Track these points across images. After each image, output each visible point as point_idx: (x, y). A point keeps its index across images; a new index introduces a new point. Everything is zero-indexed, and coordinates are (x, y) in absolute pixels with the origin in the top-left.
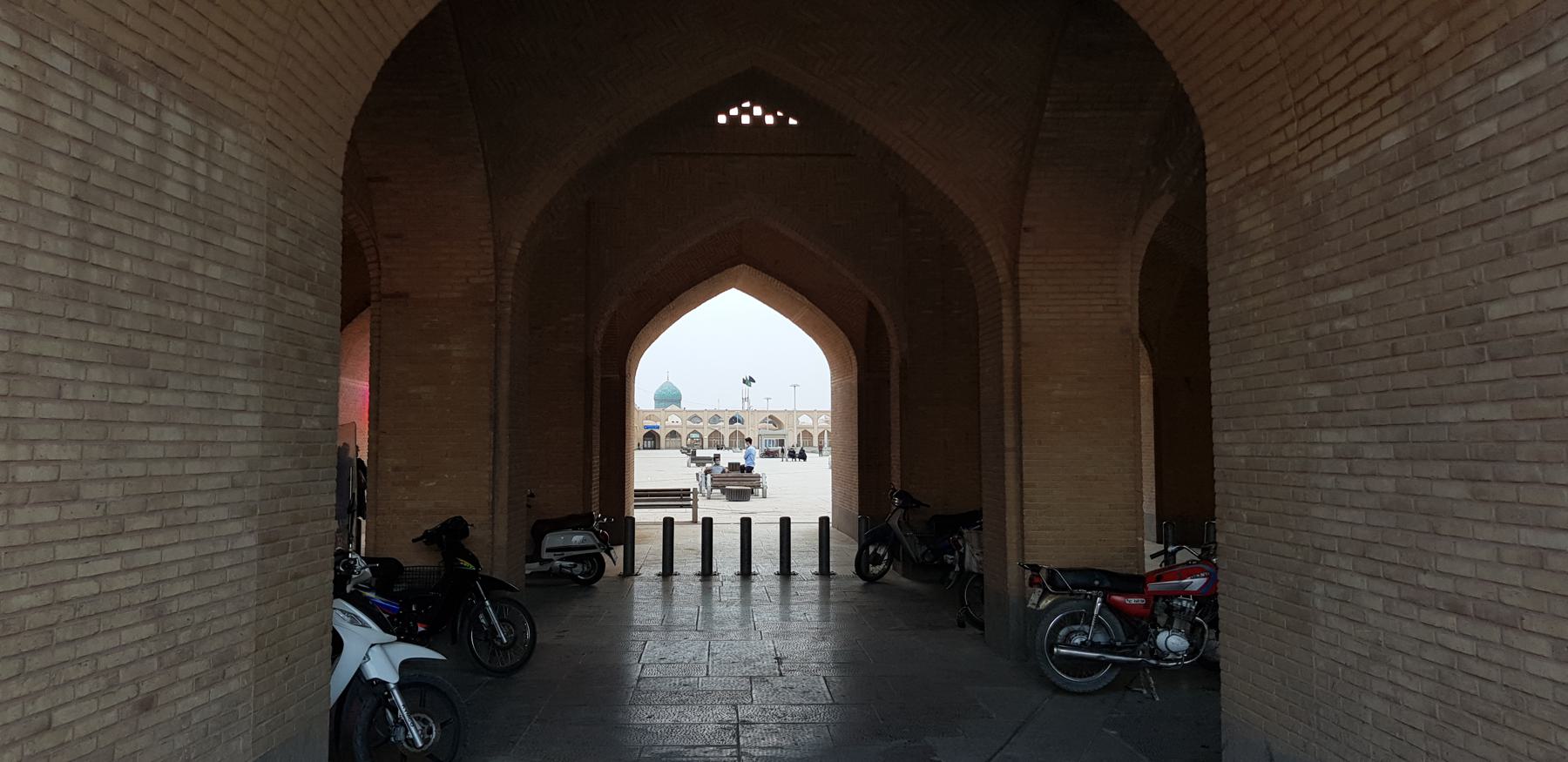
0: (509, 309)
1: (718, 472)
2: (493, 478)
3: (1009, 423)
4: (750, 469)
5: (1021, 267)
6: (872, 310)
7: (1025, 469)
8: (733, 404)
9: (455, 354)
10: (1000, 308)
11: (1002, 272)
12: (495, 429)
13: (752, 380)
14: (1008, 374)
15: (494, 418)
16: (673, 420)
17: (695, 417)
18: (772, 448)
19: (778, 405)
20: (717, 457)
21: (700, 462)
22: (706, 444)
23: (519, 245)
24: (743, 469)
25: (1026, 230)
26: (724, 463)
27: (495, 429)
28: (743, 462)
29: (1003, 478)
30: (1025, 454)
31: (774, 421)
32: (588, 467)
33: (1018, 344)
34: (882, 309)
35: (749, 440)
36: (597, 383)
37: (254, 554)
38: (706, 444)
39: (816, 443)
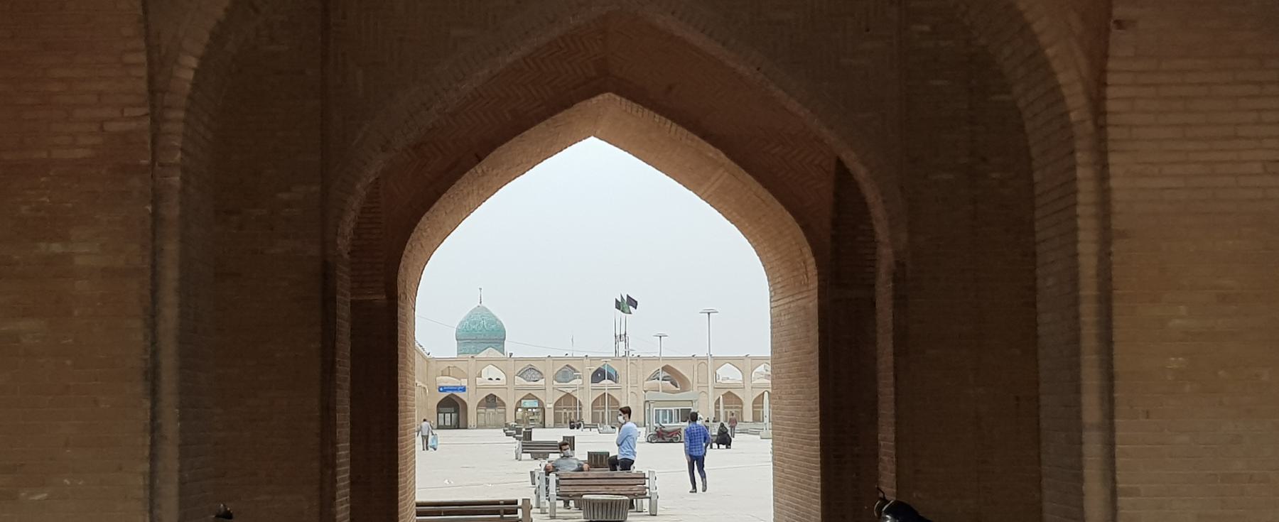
0: (176, 180)
1: (568, 469)
2: (152, 488)
3: (1091, 378)
4: (627, 464)
5: (1111, 92)
6: (843, 174)
7: (1119, 461)
8: (600, 348)
9: (79, 261)
10: (1073, 168)
11: (1071, 81)
12: (154, 393)
13: (633, 303)
14: (1088, 289)
15: (152, 376)
16: (491, 376)
17: (530, 370)
18: (669, 426)
19: (673, 349)
20: (569, 443)
21: (530, 447)
22: (550, 419)
23: (193, 62)
24: (614, 463)
25: (1120, 24)
26: (581, 454)
27: (154, 393)
28: (614, 452)
29: (1080, 478)
30: (1119, 434)
31: (672, 376)
32: (329, 463)
33: (1106, 237)
34: (860, 172)
35: (627, 411)
36: (344, 312)
37: (1038, 214)
38: (550, 419)
39: (748, 416)
